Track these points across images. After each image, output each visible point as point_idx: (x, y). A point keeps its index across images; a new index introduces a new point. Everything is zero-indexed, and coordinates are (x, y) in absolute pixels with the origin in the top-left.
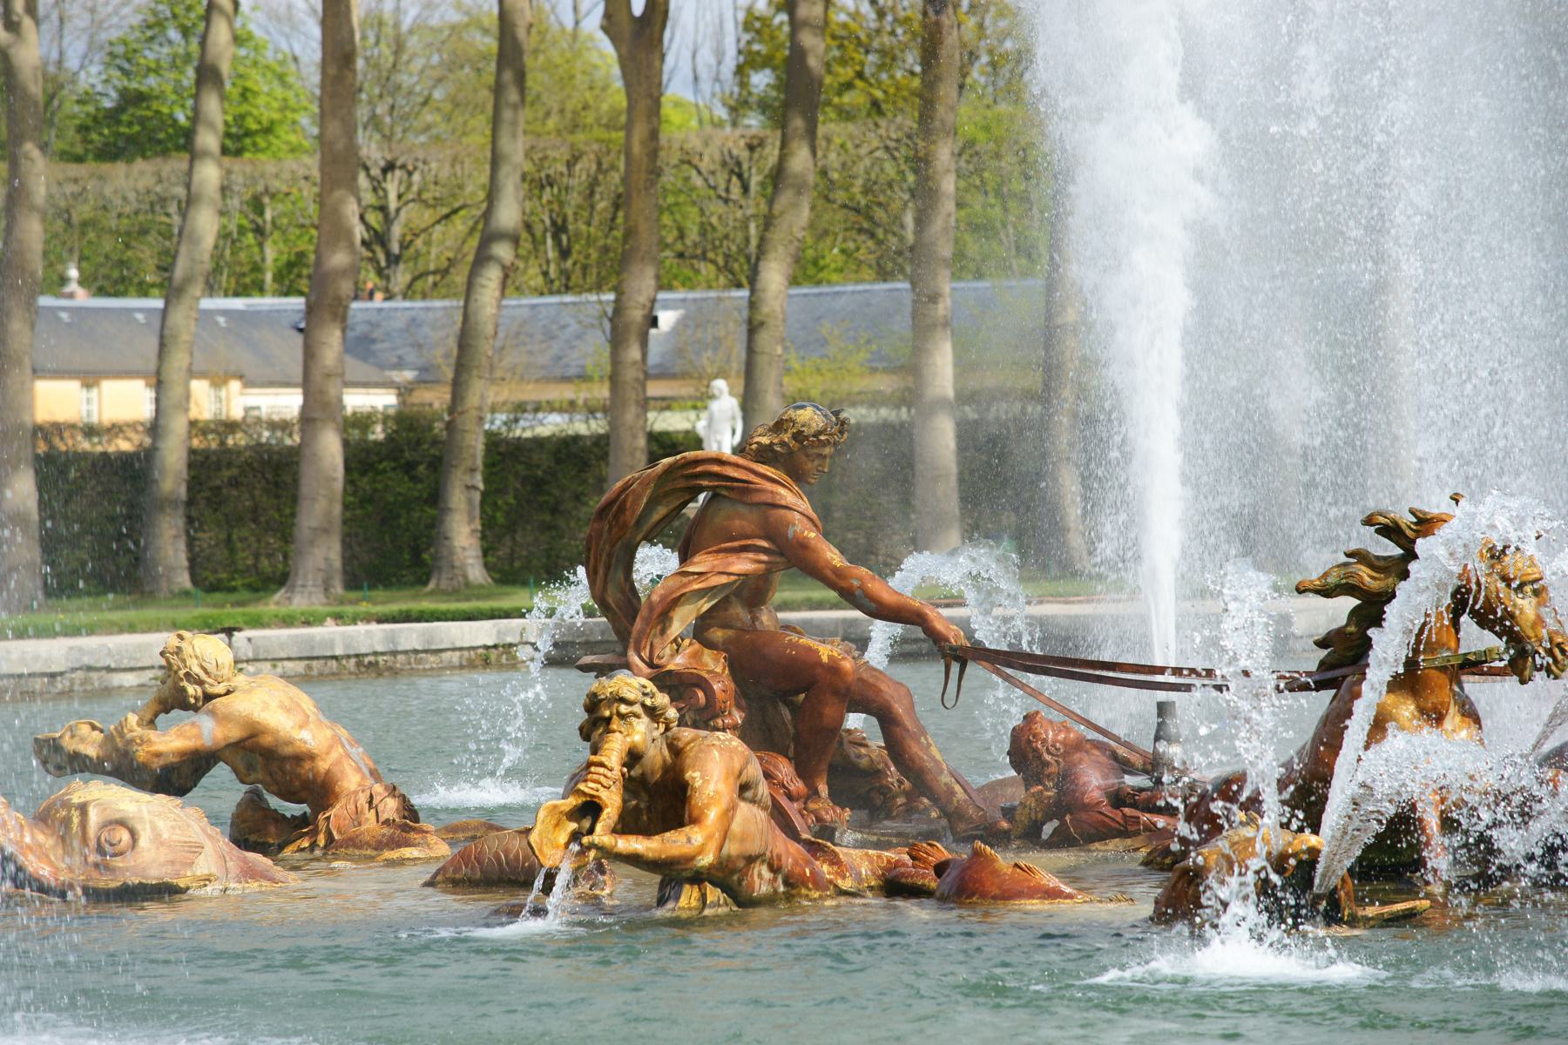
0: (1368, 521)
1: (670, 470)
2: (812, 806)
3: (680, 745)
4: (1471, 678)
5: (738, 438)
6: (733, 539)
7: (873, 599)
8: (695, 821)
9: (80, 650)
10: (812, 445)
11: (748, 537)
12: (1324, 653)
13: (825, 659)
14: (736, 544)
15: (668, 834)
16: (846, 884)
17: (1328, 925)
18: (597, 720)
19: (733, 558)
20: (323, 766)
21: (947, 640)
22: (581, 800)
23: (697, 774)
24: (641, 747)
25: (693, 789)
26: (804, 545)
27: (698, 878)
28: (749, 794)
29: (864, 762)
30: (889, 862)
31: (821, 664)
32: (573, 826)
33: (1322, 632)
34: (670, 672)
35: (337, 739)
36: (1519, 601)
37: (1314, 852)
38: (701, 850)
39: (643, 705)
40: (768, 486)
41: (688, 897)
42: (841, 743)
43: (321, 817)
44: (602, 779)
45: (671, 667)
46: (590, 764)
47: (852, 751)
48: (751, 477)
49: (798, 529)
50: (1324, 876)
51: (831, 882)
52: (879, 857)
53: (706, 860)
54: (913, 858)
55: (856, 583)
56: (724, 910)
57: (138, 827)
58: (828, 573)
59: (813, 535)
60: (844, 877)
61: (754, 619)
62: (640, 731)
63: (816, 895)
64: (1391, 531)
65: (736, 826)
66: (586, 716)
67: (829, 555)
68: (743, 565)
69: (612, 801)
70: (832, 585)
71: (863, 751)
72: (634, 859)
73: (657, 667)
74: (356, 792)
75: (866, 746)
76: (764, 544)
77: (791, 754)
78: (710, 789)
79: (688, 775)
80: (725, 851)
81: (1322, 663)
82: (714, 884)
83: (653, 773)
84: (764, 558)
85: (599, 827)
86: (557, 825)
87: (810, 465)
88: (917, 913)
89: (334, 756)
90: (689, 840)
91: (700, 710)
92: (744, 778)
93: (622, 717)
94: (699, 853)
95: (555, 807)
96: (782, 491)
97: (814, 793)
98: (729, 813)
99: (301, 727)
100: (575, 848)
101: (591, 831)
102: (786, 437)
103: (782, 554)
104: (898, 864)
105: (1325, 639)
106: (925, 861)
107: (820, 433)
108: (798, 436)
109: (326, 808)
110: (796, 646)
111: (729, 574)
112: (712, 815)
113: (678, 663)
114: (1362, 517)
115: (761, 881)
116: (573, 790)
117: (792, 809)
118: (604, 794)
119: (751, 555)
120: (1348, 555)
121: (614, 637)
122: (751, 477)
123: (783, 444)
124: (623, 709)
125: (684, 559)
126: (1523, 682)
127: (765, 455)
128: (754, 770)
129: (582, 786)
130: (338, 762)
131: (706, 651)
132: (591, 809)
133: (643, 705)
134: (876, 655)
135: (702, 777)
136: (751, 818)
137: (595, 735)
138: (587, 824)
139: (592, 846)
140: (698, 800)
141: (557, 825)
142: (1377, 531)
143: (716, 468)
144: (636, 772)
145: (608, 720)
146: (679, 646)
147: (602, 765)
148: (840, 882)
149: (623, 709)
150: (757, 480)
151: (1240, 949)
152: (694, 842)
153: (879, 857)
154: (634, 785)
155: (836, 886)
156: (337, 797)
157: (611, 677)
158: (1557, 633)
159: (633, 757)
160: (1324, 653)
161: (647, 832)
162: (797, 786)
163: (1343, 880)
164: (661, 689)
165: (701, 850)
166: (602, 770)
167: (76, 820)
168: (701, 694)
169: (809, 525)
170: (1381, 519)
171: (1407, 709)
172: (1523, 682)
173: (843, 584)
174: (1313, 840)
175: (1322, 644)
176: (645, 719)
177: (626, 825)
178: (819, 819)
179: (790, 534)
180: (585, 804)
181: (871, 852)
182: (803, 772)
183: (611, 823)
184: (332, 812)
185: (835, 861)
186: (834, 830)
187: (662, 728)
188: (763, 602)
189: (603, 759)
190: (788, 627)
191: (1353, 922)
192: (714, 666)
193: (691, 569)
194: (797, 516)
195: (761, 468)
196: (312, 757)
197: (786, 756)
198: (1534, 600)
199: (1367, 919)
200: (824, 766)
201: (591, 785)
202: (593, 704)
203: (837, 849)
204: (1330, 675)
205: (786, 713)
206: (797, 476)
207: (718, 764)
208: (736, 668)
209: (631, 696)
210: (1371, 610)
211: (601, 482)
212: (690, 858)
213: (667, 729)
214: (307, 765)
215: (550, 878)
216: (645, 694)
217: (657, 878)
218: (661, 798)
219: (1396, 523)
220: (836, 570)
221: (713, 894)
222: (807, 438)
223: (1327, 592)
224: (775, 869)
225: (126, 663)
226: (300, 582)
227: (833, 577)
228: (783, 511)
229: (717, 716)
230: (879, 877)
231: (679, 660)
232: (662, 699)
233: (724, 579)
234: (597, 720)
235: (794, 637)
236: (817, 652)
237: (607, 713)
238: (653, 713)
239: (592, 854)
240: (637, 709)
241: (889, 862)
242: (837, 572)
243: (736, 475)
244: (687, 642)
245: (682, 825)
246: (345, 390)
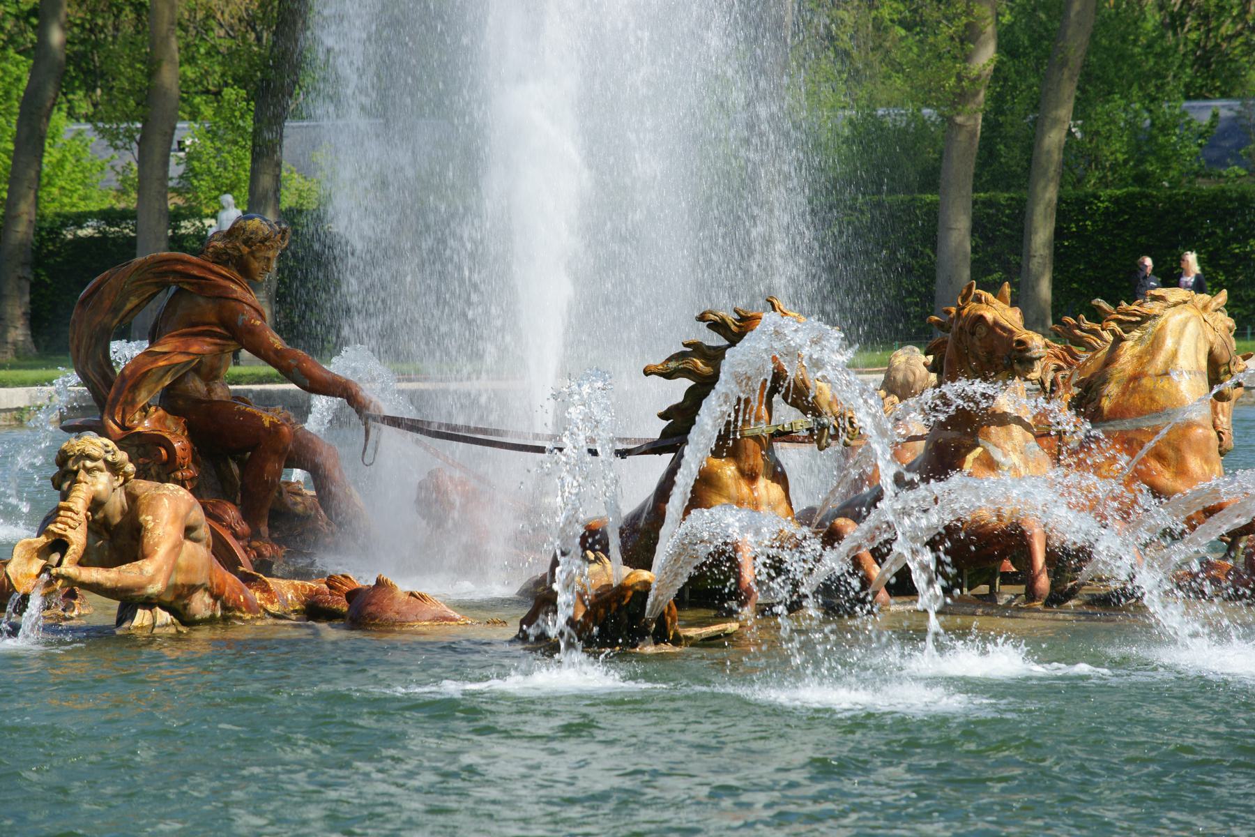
0: (702, 318)
2: (255, 544)
4: (779, 444)
7: (308, 375)
8: (144, 557)
11: (204, 324)
12: (665, 423)
13: (267, 424)
15: (124, 567)
16: (273, 608)
17: (656, 643)
18: (66, 471)
19: (192, 340)
23: (149, 518)
24: (103, 496)
27: (149, 603)
28: (193, 535)
29: (300, 508)
30: (311, 590)
32: (43, 562)
34: (139, 433)
37: (647, 585)
38: (152, 580)
39: (106, 461)
40: (227, 283)
41: (142, 617)
42: (281, 493)
44: (70, 521)
45: (139, 429)
46: (59, 509)
47: (289, 500)
50: (653, 605)
51: (261, 606)
52: (303, 586)
54: (330, 587)
56: (172, 630)
60: (272, 603)
61: (210, 391)
62: (102, 482)
63: (248, 617)
64: (718, 326)
65: (182, 561)
66: (57, 469)
67: (272, 339)
69: (78, 538)
70: (269, 361)
71: (299, 499)
72: (96, 588)
73: (129, 429)
75: (301, 495)
77: (238, 501)
78: (159, 531)
79: (142, 518)
82: (164, 608)
85: (65, 561)
87: (256, 265)
88: (330, 632)
91: (165, 464)
94: (150, 583)
95: (29, 544)
96: (234, 286)
97: (256, 535)
98: (177, 547)
100: (45, 577)
101: (59, 564)
104: (318, 592)
105: (666, 412)
106: (339, 589)
110: (242, 413)
111: (189, 354)
112: (162, 551)
113: (146, 426)
114: (697, 314)
115: (201, 604)
116: (43, 531)
117: (237, 547)
118: (70, 533)
120: (685, 345)
121: (92, 403)
125: (152, 343)
126: (821, 449)
128: (198, 515)
129: (52, 527)
131: (169, 416)
132: (60, 545)
133: (106, 461)
134: (313, 424)
135: (154, 520)
136: (198, 554)
137: (65, 486)
138: (56, 557)
139: (58, 577)
140: (149, 539)
142: (709, 326)
143: (179, 267)
144: (100, 515)
145: (77, 472)
146: (147, 412)
147: (69, 509)
148: (269, 607)
149: (89, 464)
152: (149, 573)
153: (303, 586)
154: (99, 524)
155: (265, 610)
157: (78, 437)
159: (96, 504)
160: (665, 423)
161: (106, 564)
162: (242, 527)
163: (669, 606)
164: (121, 448)
165: (152, 580)
166: (69, 514)
168: (163, 452)
170: (712, 317)
171: (728, 470)
172: (821, 449)
173: (284, 364)
174: (644, 575)
175: (663, 416)
177: (82, 563)
178: (260, 555)
179: (240, 323)
181: (296, 582)
182: (247, 515)
183: (77, 558)
185: (266, 589)
186: (271, 564)
187: (121, 480)
188: (217, 377)
189: (71, 505)
190: (238, 397)
191: (677, 641)
193: (157, 349)
194: (247, 308)
195: (217, 268)
197: (234, 503)
199: (687, 638)
200: (265, 512)
201: (59, 525)
202: (63, 459)
203: (267, 579)
204: (670, 442)
205: (235, 468)
207: (170, 509)
208: (194, 433)
209: (96, 453)
210: (703, 386)
213: (126, 481)
215: (25, 598)
216: (107, 452)
217: (117, 603)
218: (119, 538)
219: (723, 319)
220: (277, 351)
221: (164, 616)
223: (668, 375)
224: (216, 597)
228: (233, 304)
229: (178, 470)
230: (302, 603)
231: (146, 423)
232: (122, 456)
234: (66, 471)
235: (242, 407)
236: (260, 418)
238: (114, 468)
239: (60, 582)
240: (100, 464)
241: (311, 590)
243: (195, 272)
244: (153, 409)
245: (137, 560)
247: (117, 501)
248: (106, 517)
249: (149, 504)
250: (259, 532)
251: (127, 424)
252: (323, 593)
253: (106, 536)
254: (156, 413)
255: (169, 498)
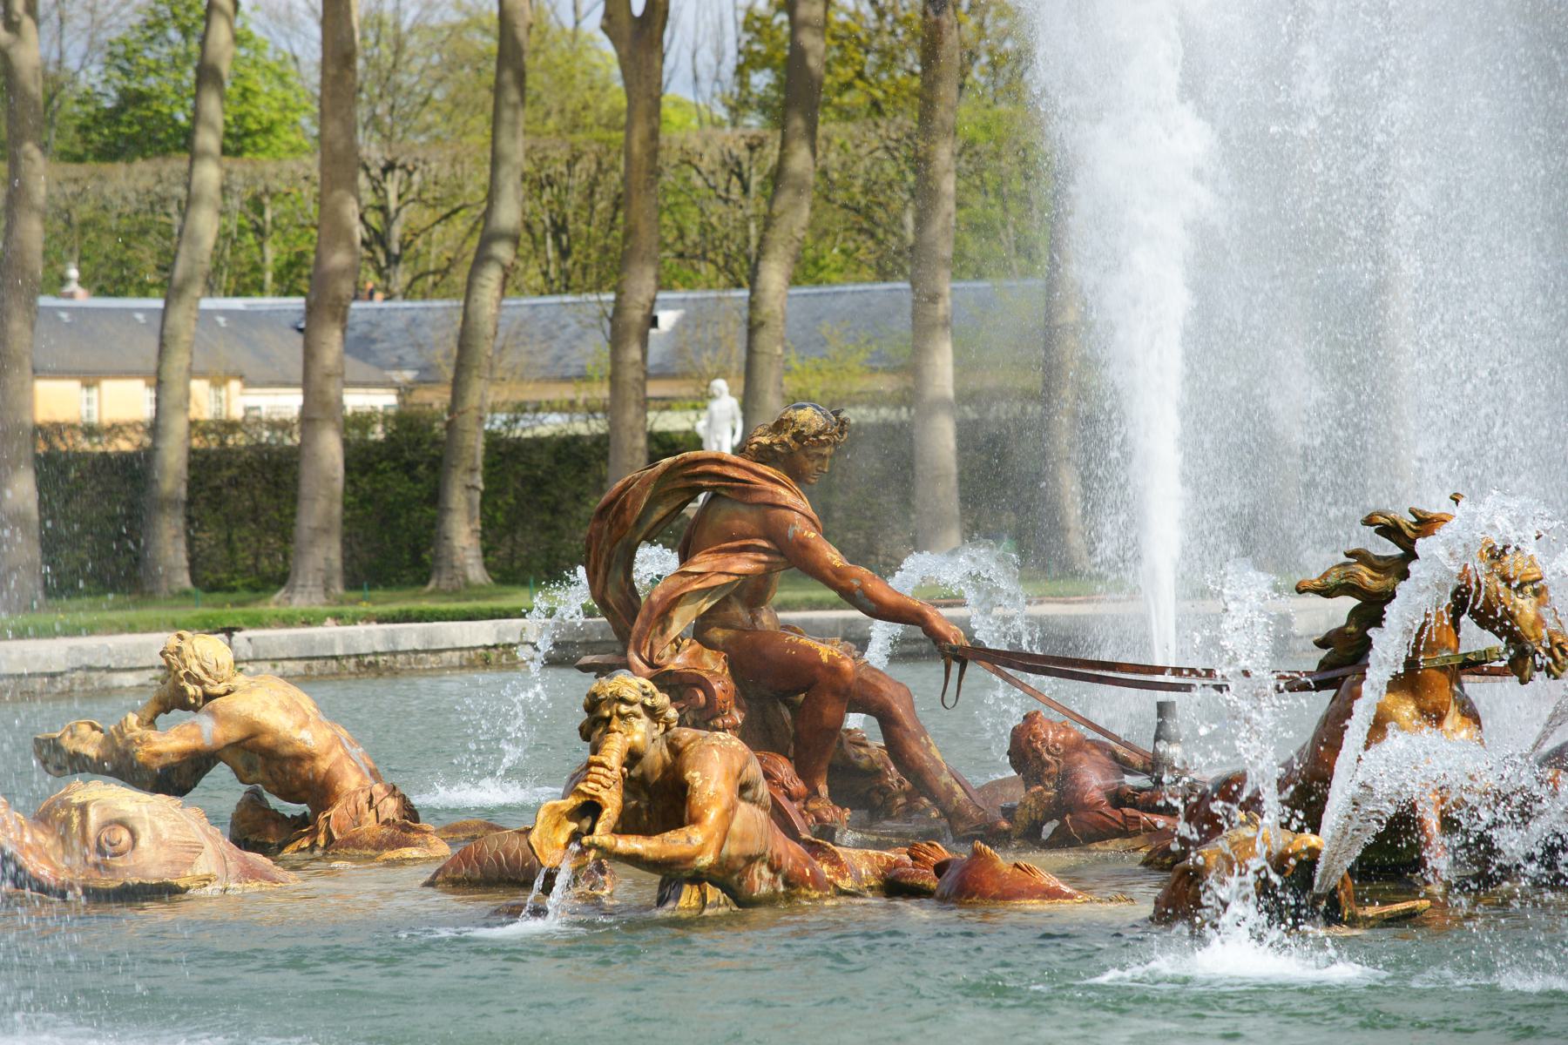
0: (1368, 521)
1: (670, 470)
2: (812, 806)
3: (680, 745)
4: (1471, 678)
5: (738, 438)
6: (733, 539)
7: (872, 599)
8: (695, 821)
9: (80, 650)
10: (812, 445)
11: (748, 537)
12: (1324, 653)
13: (825, 659)
14: (736, 544)
15: (668, 834)
16: (847, 884)
18: (597, 720)
19: (733, 558)
20: (323, 765)
21: (947, 640)
22: (581, 800)
23: (697, 774)
24: (641, 747)
25: (693, 789)
26: (804, 545)
27: (698, 878)
28: (749, 794)
29: (864, 762)
30: (889, 862)
31: (821, 664)
32: (573, 826)
33: (1322, 632)
35: (337, 739)
36: (1519, 601)
37: (1314, 852)
38: (701, 850)
39: (643, 705)
40: (768, 486)
41: (688, 897)
42: (841, 743)
43: (321, 817)
44: (602, 779)
45: (671, 667)
46: (590, 764)
47: (852, 751)
48: (751, 477)
49: (798, 528)
50: (1324, 876)
51: (831, 882)
52: (879, 857)
53: (706, 860)
54: (913, 858)
55: (856, 583)
57: (138, 827)
58: (828, 573)
59: (812, 535)
60: (844, 877)
61: (754, 619)
62: (640, 731)
63: (816, 895)
64: (1391, 531)
65: (736, 826)
66: (586, 716)
67: (829, 555)
68: (743, 565)
69: (612, 801)
70: (832, 585)
71: (863, 750)
72: (634, 859)
73: (657, 667)
74: (356, 792)
75: (866, 746)
76: (764, 544)
79: (688, 775)
80: (725, 851)
81: (1322, 663)
83: (653, 773)
84: (764, 558)
85: (599, 827)
86: (557, 825)
88: (917, 913)
89: (334, 756)
90: (689, 840)
91: (700, 710)
92: (744, 778)
93: (622, 717)
95: (555, 807)
96: (782, 491)
97: (814, 793)
98: (729, 813)
99: (301, 727)
100: (575, 848)
101: (591, 831)
102: (786, 437)
103: (782, 554)
104: (898, 864)
105: (1325, 639)
106: (924, 861)
107: (820, 433)
108: (798, 436)
109: (326, 808)
111: (730, 574)
112: (712, 815)
113: (678, 663)
115: (761, 881)
116: (573, 790)
117: (792, 809)
118: (604, 795)
119: (751, 555)
121: (614, 637)
122: (751, 477)
123: (783, 443)
124: (623, 709)
125: (684, 559)
126: (1523, 682)
127: (765, 455)
128: (754, 770)
129: (582, 786)
130: (338, 762)
131: (706, 651)
132: (591, 809)
133: (643, 705)
134: (876, 655)
135: (702, 777)
136: (751, 820)
137: (595, 735)
138: (587, 824)
139: (592, 846)
140: (698, 800)
141: (557, 825)
142: (1377, 531)
143: (716, 468)
144: (636, 772)
145: (608, 720)
146: (679, 646)
147: (602, 765)
148: (840, 882)
149: (623, 709)
150: (757, 480)
151: (1240, 949)
152: (694, 842)
153: (879, 857)
154: (634, 785)
155: (836, 886)
156: (337, 797)
157: (611, 677)
158: (1557, 633)
159: (633, 757)
160: (1324, 653)
161: (647, 832)
162: (797, 786)
163: (1343, 880)
164: (661, 689)
165: (701, 850)
166: (602, 770)
167: (76, 820)
168: (701, 694)
169: (809, 525)
170: (1381, 519)
171: (1407, 709)
172: (1523, 682)
173: (843, 584)
175: (1322, 644)
176: (645, 719)
177: (626, 825)
178: (819, 819)
179: (790, 534)
180: (585, 804)
181: (871, 852)
182: (803, 772)
184: (332, 812)
185: (835, 861)
186: (834, 830)
187: (662, 728)
188: (763, 602)
189: (603, 759)
190: (788, 627)
191: (1353, 922)
192: (714, 666)
193: (691, 569)
194: (797, 516)
195: (761, 468)
196: (312, 757)
198: (1534, 600)
200: (824, 766)
201: (591, 785)
202: (593, 704)
203: (837, 849)
204: (1330, 675)
205: (786, 713)
206: (797, 476)
207: (718, 764)
208: (736, 668)
209: (631, 696)
210: (1371, 610)
211: (601, 482)
212: (691, 858)
213: (667, 729)
214: (307, 765)
215: (550, 878)
216: (645, 694)
217: (657, 878)
218: (661, 798)
219: (1396, 523)
220: (836, 571)
221: (713, 894)
222: (807, 438)
223: (1327, 592)
224: (775, 869)
225: (125, 663)
226: (300, 582)
227: (833, 577)
228: (783, 512)
229: (717, 716)
230: (879, 877)
231: (679, 660)
232: (662, 699)
233: (724, 579)
234: (597, 720)
235: (794, 637)
236: (817, 652)
237: (607, 713)
238: (653, 713)
239: (592, 854)
240: (637, 709)
241: (889, 862)
242: (837, 572)
243: (736, 475)
244: (687, 642)
245: (682, 825)
246: (345, 390)
247: (657, 754)
248: (643, 775)
249: (696, 758)
250: (816, 793)
251: (656, 661)
252: (904, 865)
253: (645, 796)
254: (690, 647)
255: (720, 749)
